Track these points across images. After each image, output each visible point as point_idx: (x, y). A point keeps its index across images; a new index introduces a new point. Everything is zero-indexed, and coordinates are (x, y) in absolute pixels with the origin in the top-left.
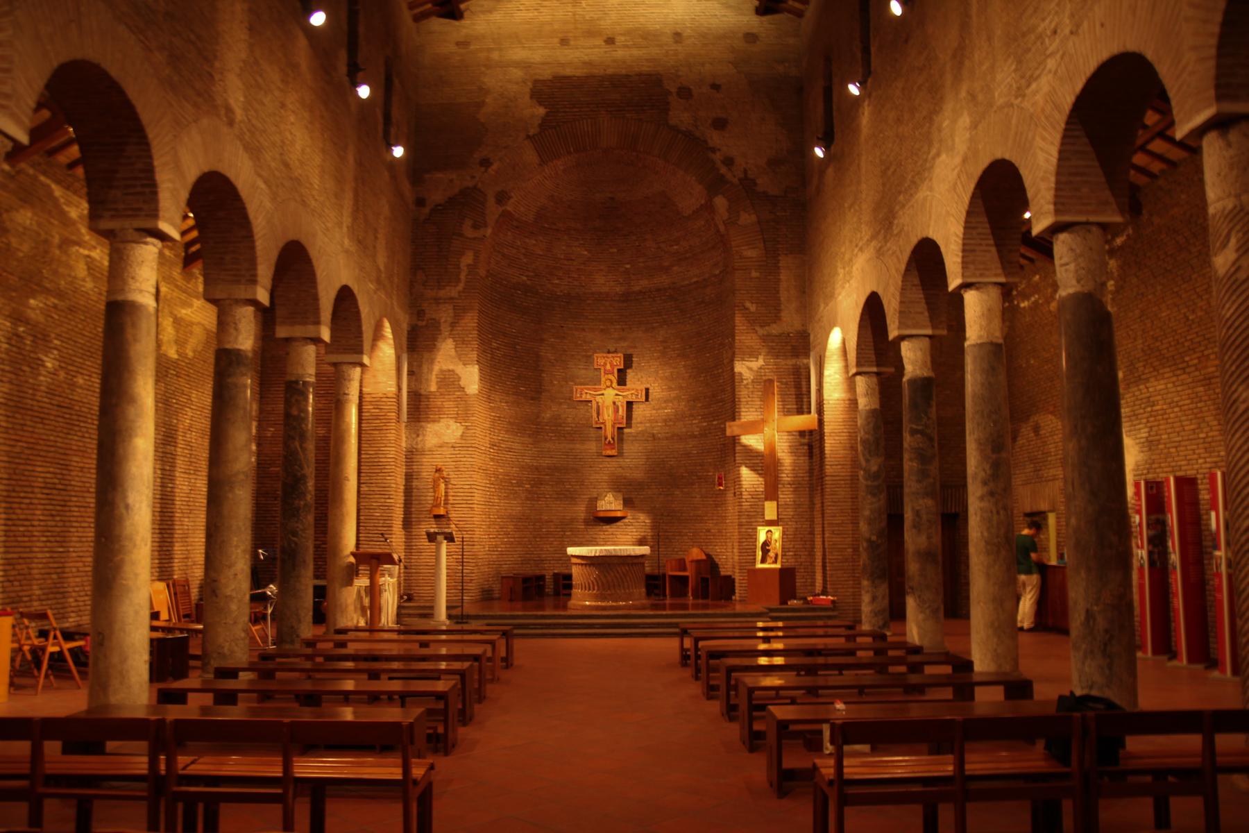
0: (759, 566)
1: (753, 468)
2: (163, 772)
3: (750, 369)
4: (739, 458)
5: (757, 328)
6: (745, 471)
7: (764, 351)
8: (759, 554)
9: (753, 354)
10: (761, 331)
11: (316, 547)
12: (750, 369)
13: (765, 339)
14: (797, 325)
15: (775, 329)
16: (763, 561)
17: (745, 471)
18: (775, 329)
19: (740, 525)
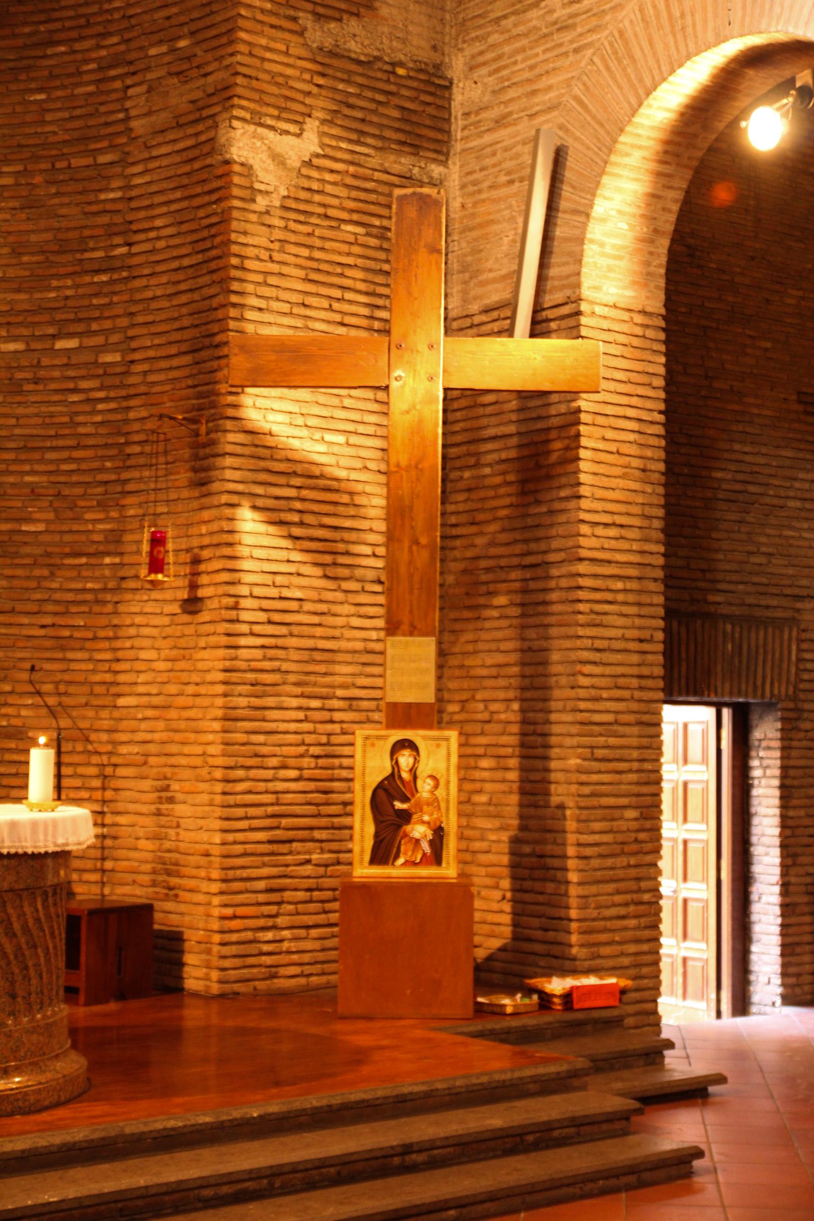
0: (364, 871)
1: (276, 517)
2: (690, 730)
3: (279, 159)
4: (231, 472)
5: (306, 20)
6: (250, 524)
7: (321, 105)
8: (364, 829)
9: (289, 112)
10: (318, 35)
11: (547, 1127)
12: (279, 159)
13: (329, 61)
14: (418, 47)
15: (356, 38)
16: (382, 853)
17: (250, 524)
18: (356, 38)
19: (229, 718)
